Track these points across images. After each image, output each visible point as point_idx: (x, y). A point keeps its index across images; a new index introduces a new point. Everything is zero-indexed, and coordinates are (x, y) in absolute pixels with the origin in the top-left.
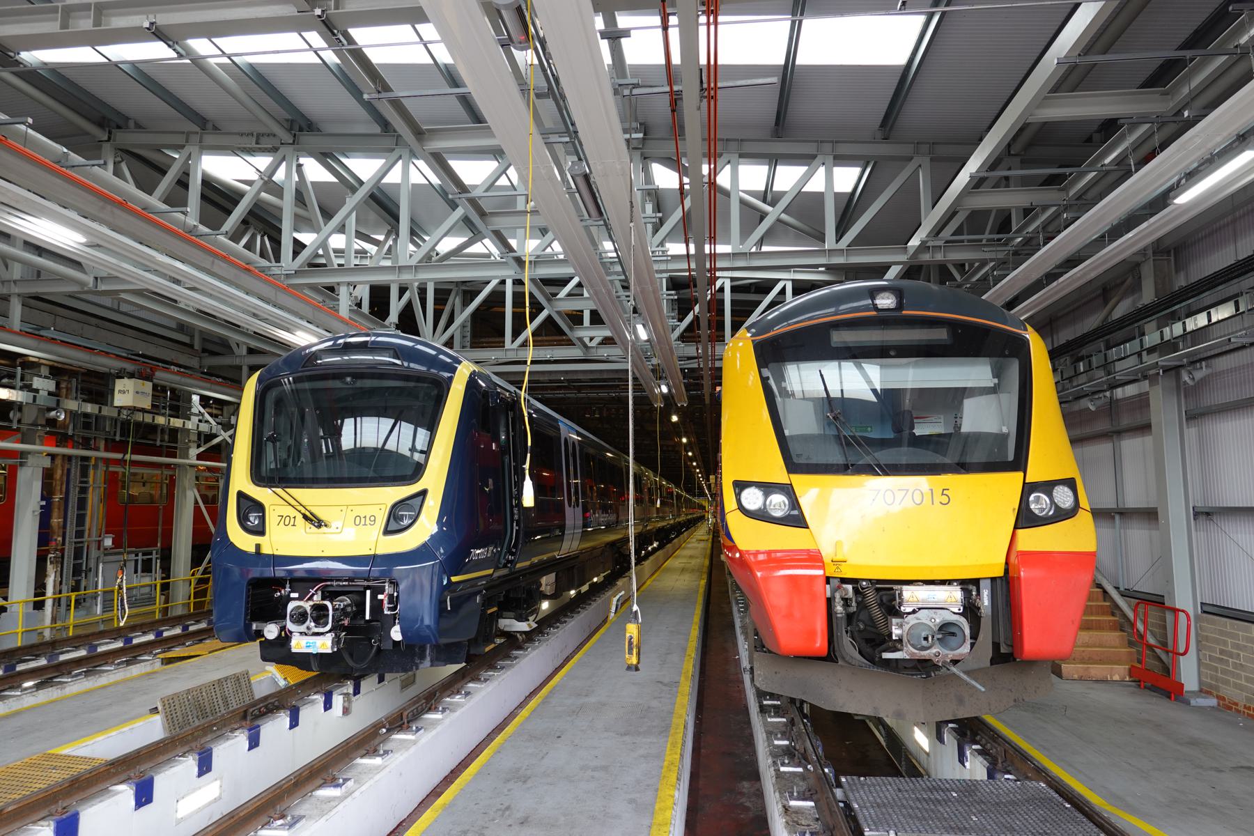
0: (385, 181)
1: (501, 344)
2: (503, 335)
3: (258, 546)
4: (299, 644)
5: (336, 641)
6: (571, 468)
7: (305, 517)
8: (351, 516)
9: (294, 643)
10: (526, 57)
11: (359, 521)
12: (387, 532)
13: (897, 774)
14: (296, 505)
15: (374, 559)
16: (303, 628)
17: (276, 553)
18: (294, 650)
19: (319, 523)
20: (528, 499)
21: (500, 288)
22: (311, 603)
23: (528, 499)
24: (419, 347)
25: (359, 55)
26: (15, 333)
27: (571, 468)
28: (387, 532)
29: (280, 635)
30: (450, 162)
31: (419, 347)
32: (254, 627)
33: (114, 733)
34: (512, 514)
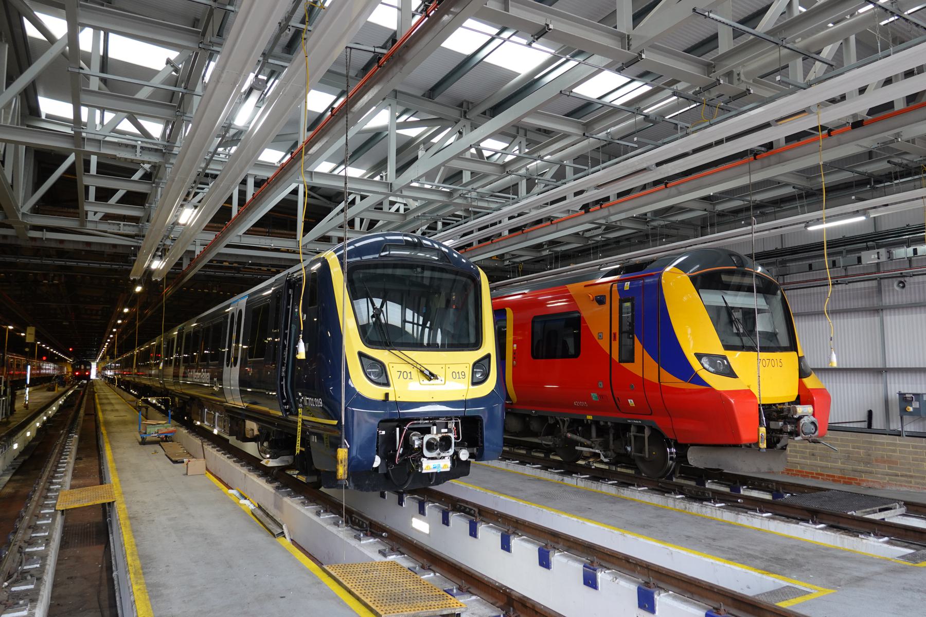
1: (294, 237)
2: (295, 230)
3: (387, 395)
6: (234, 335)
12: (695, 354)
13: (212, 221)
14: (414, 364)
17: (398, 400)
18: (448, 470)
19: (431, 376)
20: (302, 354)
21: (293, 197)
22: (440, 435)
23: (302, 354)
24: (357, 245)
27: (234, 335)
31: (357, 245)
33: (575, 519)
34: (286, 372)
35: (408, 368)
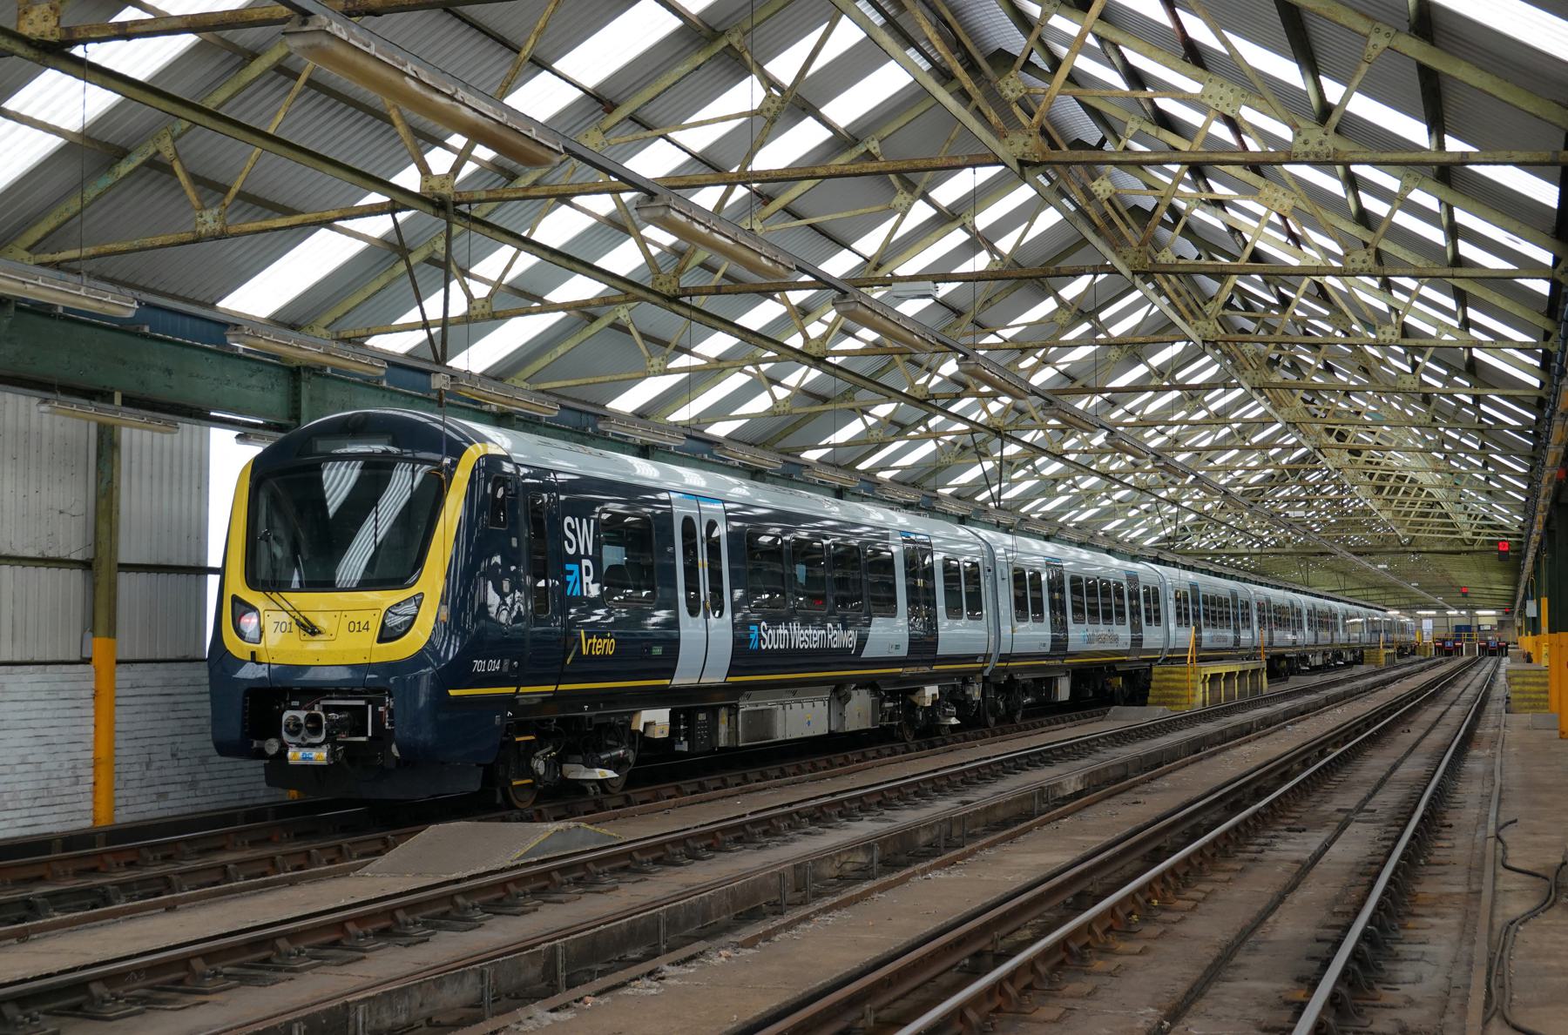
0: (442, 291)
4: (295, 755)
5: (332, 754)
7: (298, 623)
8: (345, 622)
9: (290, 754)
10: (1064, 690)
11: (358, 627)
12: (381, 640)
15: (370, 667)
16: (297, 740)
25: (974, 423)
26: (1078, 163)
28: (381, 640)
29: (769, 96)
30: (603, 287)
32: (255, 744)
35: (285, 617)
